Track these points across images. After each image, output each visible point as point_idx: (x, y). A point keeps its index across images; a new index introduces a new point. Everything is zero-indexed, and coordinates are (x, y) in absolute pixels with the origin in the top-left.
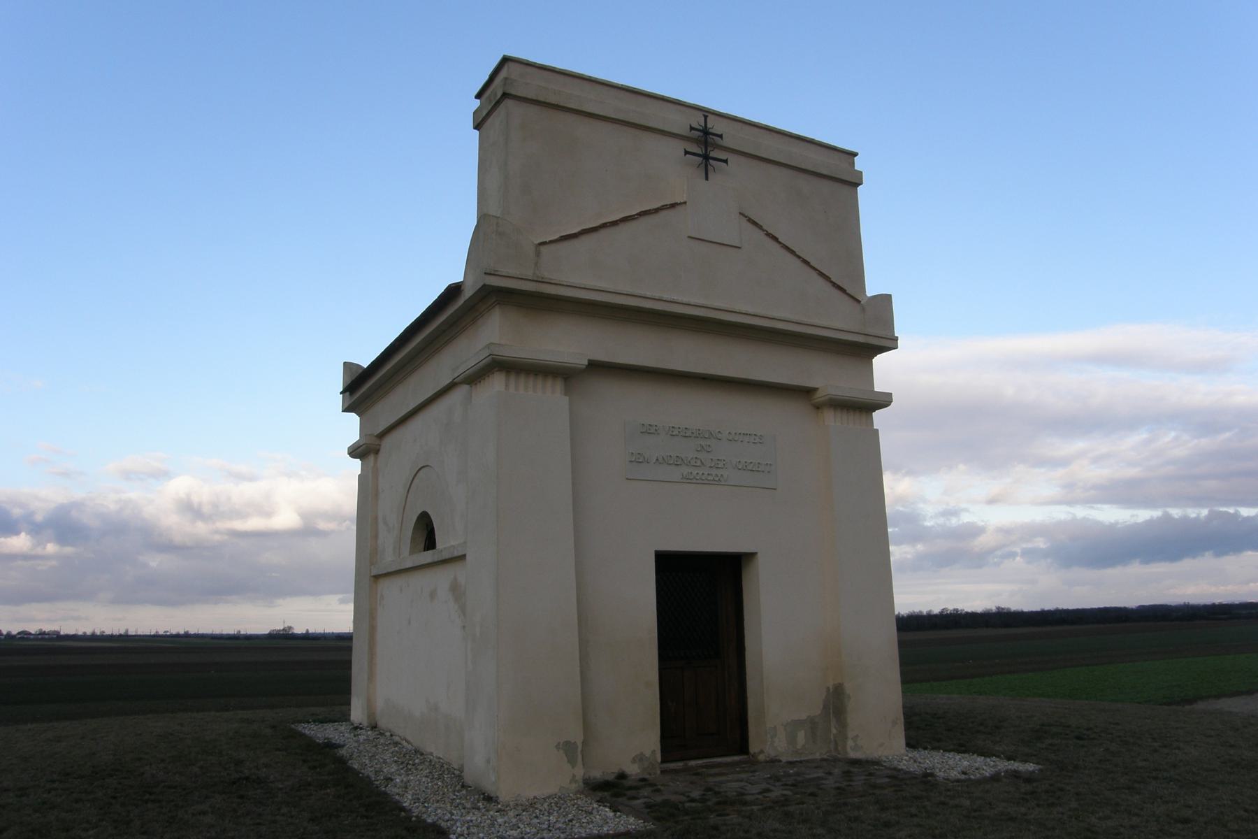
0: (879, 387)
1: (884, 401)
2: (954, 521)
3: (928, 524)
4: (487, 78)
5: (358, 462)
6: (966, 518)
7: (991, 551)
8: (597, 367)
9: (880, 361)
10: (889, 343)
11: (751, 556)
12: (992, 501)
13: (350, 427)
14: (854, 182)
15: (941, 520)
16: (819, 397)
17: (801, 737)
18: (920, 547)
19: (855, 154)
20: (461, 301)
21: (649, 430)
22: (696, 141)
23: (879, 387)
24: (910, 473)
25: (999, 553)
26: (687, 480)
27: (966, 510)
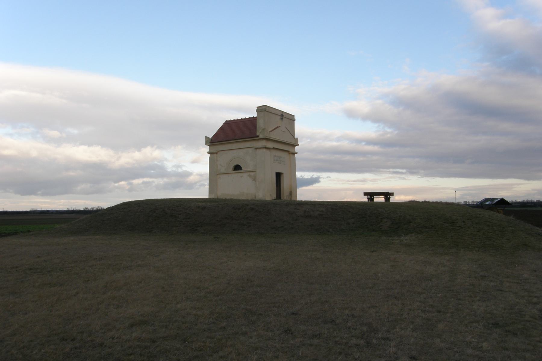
0: (296, 151)
1: (296, 153)
2: (180, 170)
3: (169, 170)
4: (260, 106)
5: (209, 154)
6: (184, 169)
7: (196, 183)
8: (274, 148)
9: (296, 147)
10: (298, 145)
11: (282, 173)
12: (194, 162)
13: (207, 149)
14: (294, 120)
15: (174, 169)
16: (290, 152)
17: (287, 197)
18: (165, 180)
19: (294, 116)
20: (258, 138)
21: (275, 156)
22: (281, 116)
23: (296, 151)
24: (159, 148)
25: (198, 184)
26: (279, 163)
27: (184, 166)
